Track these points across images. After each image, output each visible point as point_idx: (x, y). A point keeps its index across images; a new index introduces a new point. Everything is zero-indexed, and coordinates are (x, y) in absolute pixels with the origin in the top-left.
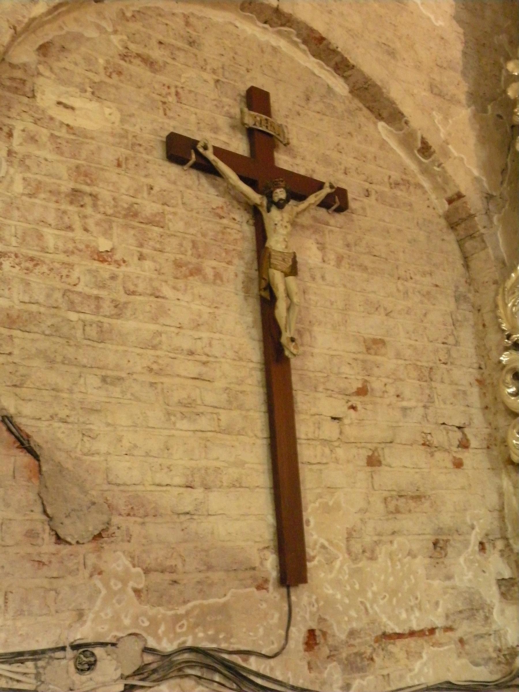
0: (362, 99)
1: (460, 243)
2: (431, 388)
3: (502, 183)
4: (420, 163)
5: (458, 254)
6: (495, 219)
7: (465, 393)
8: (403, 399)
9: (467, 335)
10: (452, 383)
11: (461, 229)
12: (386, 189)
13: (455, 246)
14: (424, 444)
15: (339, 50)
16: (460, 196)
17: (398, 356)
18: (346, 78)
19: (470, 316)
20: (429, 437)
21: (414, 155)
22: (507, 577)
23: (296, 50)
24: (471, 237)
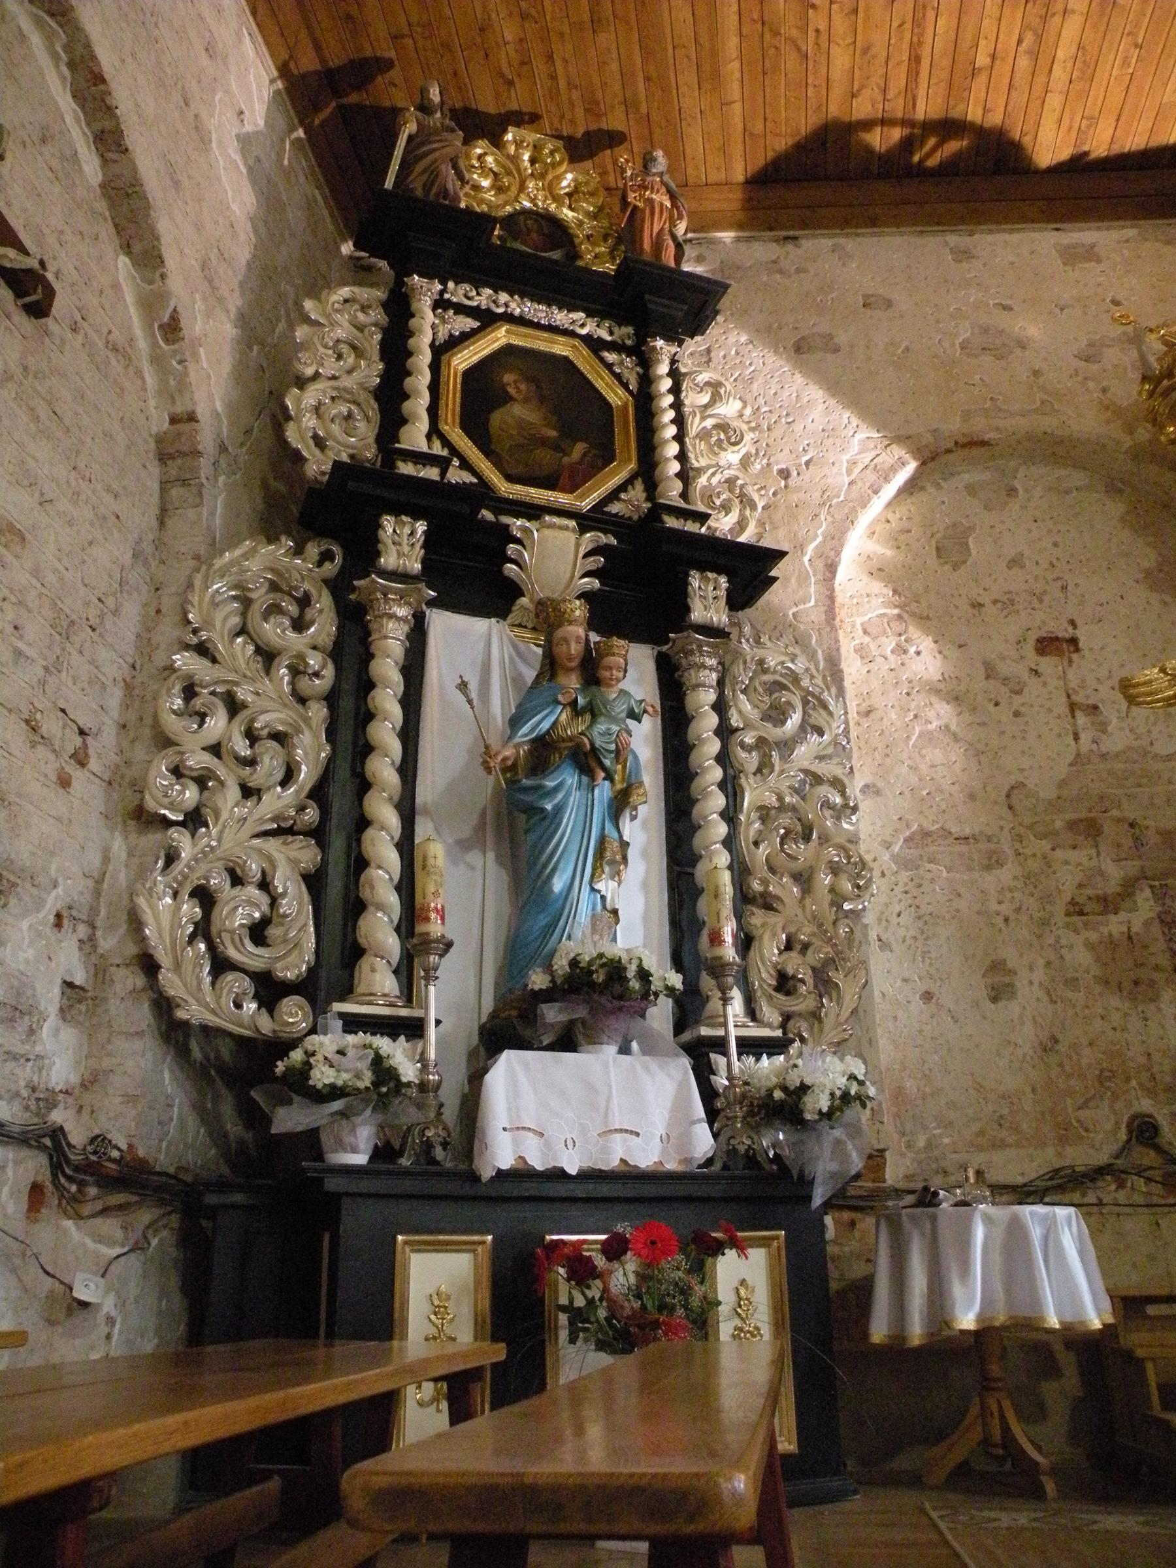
0: (112, 205)
1: (165, 486)
2: (63, 649)
3: (242, 444)
4: (154, 345)
5: (155, 500)
6: (222, 479)
7: (104, 687)
8: (21, 638)
9: (132, 610)
10: (92, 662)
11: (173, 469)
12: (101, 344)
13: (156, 486)
14: (27, 722)
15: (118, 112)
16: (192, 418)
17: (36, 572)
18: (105, 162)
19: (144, 588)
20: (38, 716)
21: (151, 327)
22: (77, 983)
23: (52, 68)
24: (185, 482)
